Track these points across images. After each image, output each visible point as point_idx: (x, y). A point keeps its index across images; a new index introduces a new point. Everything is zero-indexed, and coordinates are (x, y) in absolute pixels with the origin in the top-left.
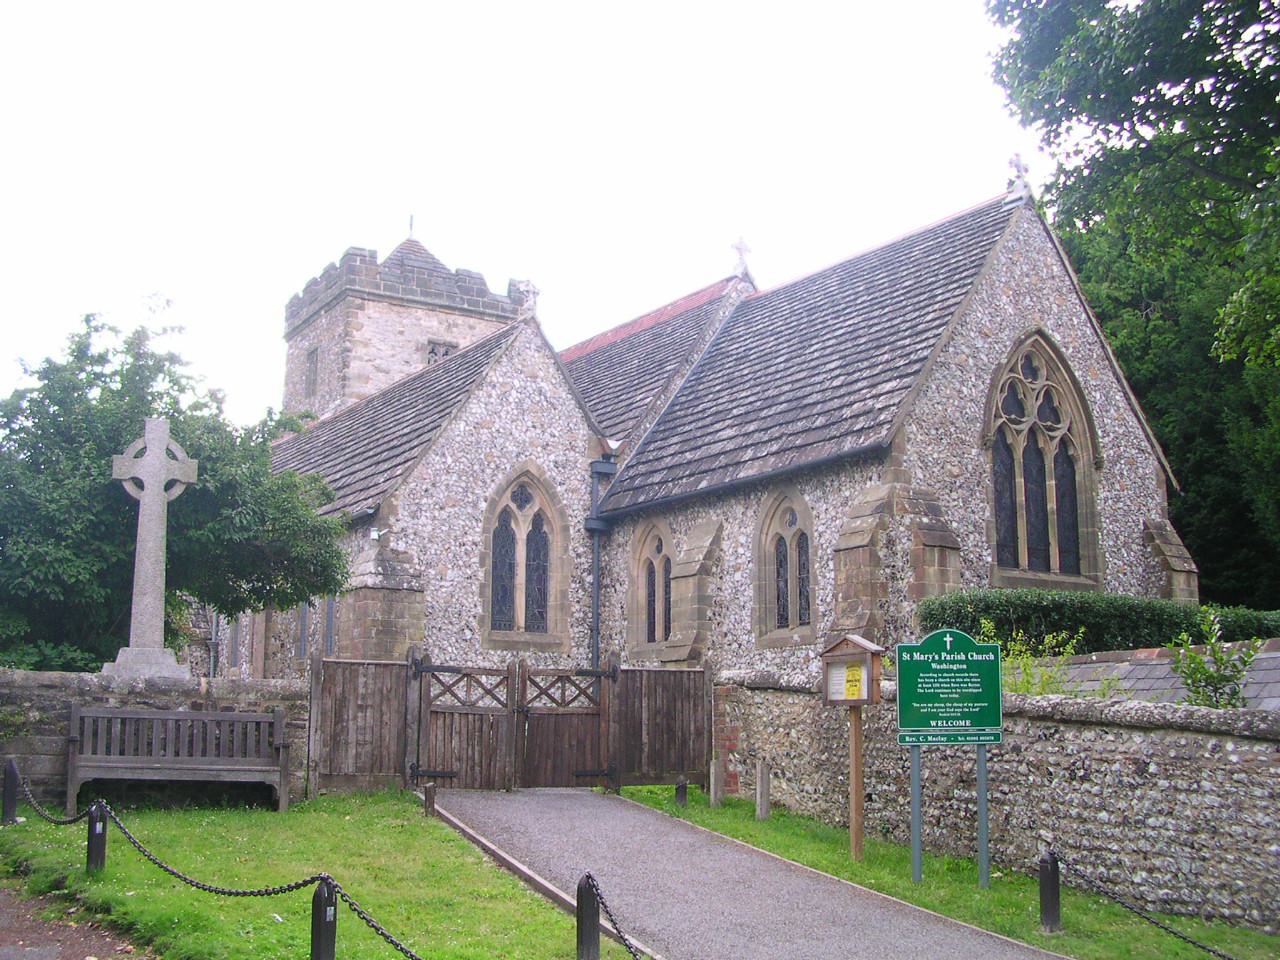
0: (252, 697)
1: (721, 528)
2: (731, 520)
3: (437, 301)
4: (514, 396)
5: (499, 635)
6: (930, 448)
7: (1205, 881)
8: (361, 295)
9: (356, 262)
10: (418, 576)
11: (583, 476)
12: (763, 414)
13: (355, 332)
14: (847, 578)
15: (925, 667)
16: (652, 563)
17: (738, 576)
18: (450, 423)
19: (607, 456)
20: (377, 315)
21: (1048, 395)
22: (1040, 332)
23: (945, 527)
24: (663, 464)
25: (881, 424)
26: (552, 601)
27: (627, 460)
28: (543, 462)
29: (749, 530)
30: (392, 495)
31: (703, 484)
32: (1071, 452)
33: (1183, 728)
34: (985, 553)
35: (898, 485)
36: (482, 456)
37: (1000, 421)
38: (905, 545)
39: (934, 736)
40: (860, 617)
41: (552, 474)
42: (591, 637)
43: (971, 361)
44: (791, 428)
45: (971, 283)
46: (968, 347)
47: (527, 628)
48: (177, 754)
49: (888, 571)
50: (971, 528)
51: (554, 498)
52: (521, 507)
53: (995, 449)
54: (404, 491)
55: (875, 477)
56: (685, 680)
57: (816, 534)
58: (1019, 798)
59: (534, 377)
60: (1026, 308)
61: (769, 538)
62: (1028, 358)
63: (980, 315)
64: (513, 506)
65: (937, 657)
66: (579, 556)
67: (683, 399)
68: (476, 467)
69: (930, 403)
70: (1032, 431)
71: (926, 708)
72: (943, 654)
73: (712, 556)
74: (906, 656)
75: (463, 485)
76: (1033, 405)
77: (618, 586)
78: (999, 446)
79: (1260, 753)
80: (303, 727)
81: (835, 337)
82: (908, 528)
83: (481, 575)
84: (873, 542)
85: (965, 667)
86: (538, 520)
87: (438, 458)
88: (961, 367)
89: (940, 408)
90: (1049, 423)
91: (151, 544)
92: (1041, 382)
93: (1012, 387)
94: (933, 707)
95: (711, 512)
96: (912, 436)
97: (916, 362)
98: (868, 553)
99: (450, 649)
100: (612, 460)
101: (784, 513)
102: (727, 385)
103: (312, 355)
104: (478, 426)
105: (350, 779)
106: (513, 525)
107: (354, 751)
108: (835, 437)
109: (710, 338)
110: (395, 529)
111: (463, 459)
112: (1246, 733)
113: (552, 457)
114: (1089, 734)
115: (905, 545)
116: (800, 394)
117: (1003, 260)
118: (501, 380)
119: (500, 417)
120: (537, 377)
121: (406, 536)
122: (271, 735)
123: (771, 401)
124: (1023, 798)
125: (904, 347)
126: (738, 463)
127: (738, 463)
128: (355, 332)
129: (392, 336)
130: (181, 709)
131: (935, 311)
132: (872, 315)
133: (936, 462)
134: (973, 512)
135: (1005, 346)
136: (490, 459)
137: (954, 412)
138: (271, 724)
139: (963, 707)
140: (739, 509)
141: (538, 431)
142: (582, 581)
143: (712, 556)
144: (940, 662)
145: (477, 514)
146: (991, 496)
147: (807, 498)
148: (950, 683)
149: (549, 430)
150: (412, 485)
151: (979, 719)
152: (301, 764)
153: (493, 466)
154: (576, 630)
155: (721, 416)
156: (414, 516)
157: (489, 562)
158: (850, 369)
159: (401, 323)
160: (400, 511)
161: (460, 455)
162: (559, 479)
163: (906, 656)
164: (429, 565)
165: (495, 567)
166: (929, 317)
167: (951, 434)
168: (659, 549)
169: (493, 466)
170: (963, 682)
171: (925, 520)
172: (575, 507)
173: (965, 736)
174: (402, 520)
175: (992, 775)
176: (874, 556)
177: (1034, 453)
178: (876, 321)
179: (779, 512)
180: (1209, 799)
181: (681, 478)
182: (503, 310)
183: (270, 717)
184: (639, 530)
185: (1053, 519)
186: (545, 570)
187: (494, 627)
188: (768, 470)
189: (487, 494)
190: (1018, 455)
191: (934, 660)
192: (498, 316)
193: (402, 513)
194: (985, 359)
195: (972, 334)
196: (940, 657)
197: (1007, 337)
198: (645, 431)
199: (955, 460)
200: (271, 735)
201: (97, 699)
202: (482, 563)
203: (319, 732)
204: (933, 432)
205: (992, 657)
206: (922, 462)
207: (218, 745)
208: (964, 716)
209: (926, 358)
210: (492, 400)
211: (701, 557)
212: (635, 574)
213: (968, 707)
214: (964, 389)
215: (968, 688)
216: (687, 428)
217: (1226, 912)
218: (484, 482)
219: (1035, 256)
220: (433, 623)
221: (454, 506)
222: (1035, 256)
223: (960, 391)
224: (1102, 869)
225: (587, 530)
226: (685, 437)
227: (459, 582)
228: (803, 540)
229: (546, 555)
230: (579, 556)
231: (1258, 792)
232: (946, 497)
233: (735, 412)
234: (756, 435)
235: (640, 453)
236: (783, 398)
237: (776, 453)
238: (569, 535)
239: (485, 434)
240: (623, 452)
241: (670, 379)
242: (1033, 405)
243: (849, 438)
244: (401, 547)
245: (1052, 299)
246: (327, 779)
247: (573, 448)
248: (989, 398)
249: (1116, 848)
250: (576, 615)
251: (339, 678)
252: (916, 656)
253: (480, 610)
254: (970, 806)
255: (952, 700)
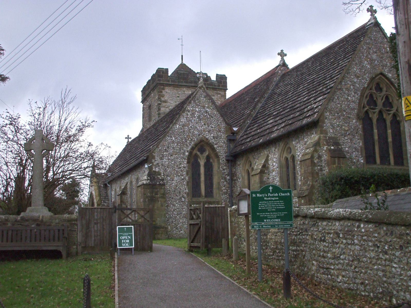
0: (57, 221)
1: (268, 156)
2: (271, 153)
3: (190, 85)
4: (196, 114)
5: (195, 200)
6: (335, 121)
7: (357, 281)
8: (162, 85)
9: (161, 73)
10: (163, 180)
11: (224, 141)
12: (282, 113)
13: (162, 98)
14: (305, 171)
15: (262, 199)
16: (248, 171)
17: (274, 173)
18: (173, 126)
19: (234, 133)
20: (169, 91)
21: (387, 98)
22: (381, 74)
23: (341, 150)
24: (251, 135)
25: (315, 113)
26: (215, 186)
27: (241, 134)
28: (210, 137)
29: (276, 156)
30: (153, 152)
31: (261, 141)
32: (398, 119)
33: (348, 219)
34: (360, 159)
35: (322, 135)
36: (186, 136)
37: (366, 109)
38: (325, 157)
39: (265, 225)
40: (309, 185)
41: (212, 141)
42: (230, 199)
43: (352, 87)
44: (289, 118)
45: (351, 58)
46: (350, 82)
47: (206, 196)
48: (31, 241)
49: (319, 167)
50: (354, 150)
51: (213, 149)
52: (202, 153)
53: (363, 119)
54: (157, 150)
55: (314, 133)
56: (217, 210)
57: (297, 156)
58: (307, 249)
59: (204, 107)
60: (376, 65)
61: (283, 159)
62: (378, 84)
63: (355, 69)
64: (198, 153)
65: (266, 195)
66: (224, 170)
67: (261, 111)
68: (183, 140)
69: (334, 104)
70: (380, 112)
71: (262, 215)
72: (269, 194)
73: (265, 166)
74: (254, 195)
75: (179, 147)
76: (380, 103)
77: (239, 180)
78: (365, 120)
79: (370, 228)
80: (75, 231)
81: (307, 83)
82: (326, 151)
83: (187, 178)
84: (312, 157)
85: (278, 198)
86: (208, 158)
87: (169, 138)
88: (348, 89)
89: (339, 105)
90: (388, 108)
91: (38, 172)
92: (384, 93)
93: (371, 96)
94: (265, 214)
95: (265, 150)
96: (327, 117)
97: (329, 89)
98: (311, 161)
99: (176, 205)
100: (235, 135)
101: (287, 150)
102: (274, 104)
103: (150, 107)
104: (184, 126)
105: (93, 248)
106: (199, 160)
107: (93, 238)
108: (301, 119)
109: (271, 88)
110: (155, 164)
111: (179, 138)
112: (366, 220)
113: (212, 135)
114: (325, 223)
115: (325, 157)
116: (293, 105)
117: (365, 47)
118: (191, 109)
119: (192, 122)
120: (205, 107)
121: (159, 166)
122: (63, 234)
123: (285, 109)
124: (308, 249)
125: (327, 84)
126: (272, 132)
127: (272, 132)
128: (162, 98)
129: (175, 98)
130: (33, 226)
131: (338, 70)
132: (319, 74)
133: (338, 126)
134: (355, 144)
135: (367, 80)
136: (188, 137)
137: (345, 107)
138: (63, 230)
139: (277, 214)
140: (273, 149)
141: (206, 126)
142: (225, 179)
143: (265, 166)
144: (268, 197)
145: (185, 157)
146: (362, 137)
147: (294, 143)
148: (272, 205)
149: (210, 126)
150: (160, 148)
151: (283, 219)
152: (75, 243)
153: (190, 139)
154: (224, 196)
155: (270, 116)
156: (161, 159)
157: (190, 174)
158: (310, 94)
159: (178, 93)
160: (156, 157)
161: (177, 136)
162: (215, 142)
163: (254, 195)
164: (167, 176)
165: (193, 174)
166: (336, 72)
167: (344, 115)
168: (251, 165)
169: (190, 139)
170: (279, 205)
171: (332, 148)
172: (222, 152)
173: (278, 225)
174: (157, 160)
175: (300, 241)
176: (312, 162)
177: (381, 120)
178: (320, 76)
179: (286, 149)
180: (357, 247)
181: (255, 139)
182: (215, 86)
183: (63, 228)
184: (244, 159)
185: (391, 145)
186: (212, 175)
187: (193, 197)
188: (280, 134)
189: (188, 150)
190: (375, 121)
191: (265, 197)
192: (213, 88)
193: (157, 158)
194: (358, 86)
195: (352, 77)
196: (268, 195)
197: (367, 77)
198: (247, 124)
199: (346, 125)
200: (63, 234)
201: (4, 224)
202: (187, 174)
203: (81, 232)
204: (336, 115)
205: (289, 194)
206: (332, 126)
207: (45, 238)
208: (278, 218)
209: (332, 87)
210: (189, 116)
211: (261, 167)
212: (243, 175)
213: (279, 214)
214: (349, 98)
215: (279, 207)
216: (260, 121)
217: (363, 293)
218: (187, 145)
219: (379, 45)
220: (170, 196)
221: (176, 155)
222: (379, 45)
223: (347, 99)
224: (329, 276)
225: (227, 160)
226: (259, 124)
227: (179, 181)
228: (293, 157)
229: (212, 170)
230: (224, 170)
231: (370, 244)
232: (343, 139)
233: (274, 114)
234: (279, 121)
235: (246, 131)
236: (288, 107)
237: (283, 127)
238: (220, 162)
239: (186, 129)
240: (239, 132)
241: (256, 105)
242: (380, 103)
243: (305, 119)
244: (157, 170)
245: (387, 61)
246: (85, 248)
247: (220, 131)
248: (360, 100)
249: (333, 268)
250: (224, 191)
251: (88, 213)
252: (258, 195)
253: (187, 191)
254: (294, 253)
255: (273, 212)
